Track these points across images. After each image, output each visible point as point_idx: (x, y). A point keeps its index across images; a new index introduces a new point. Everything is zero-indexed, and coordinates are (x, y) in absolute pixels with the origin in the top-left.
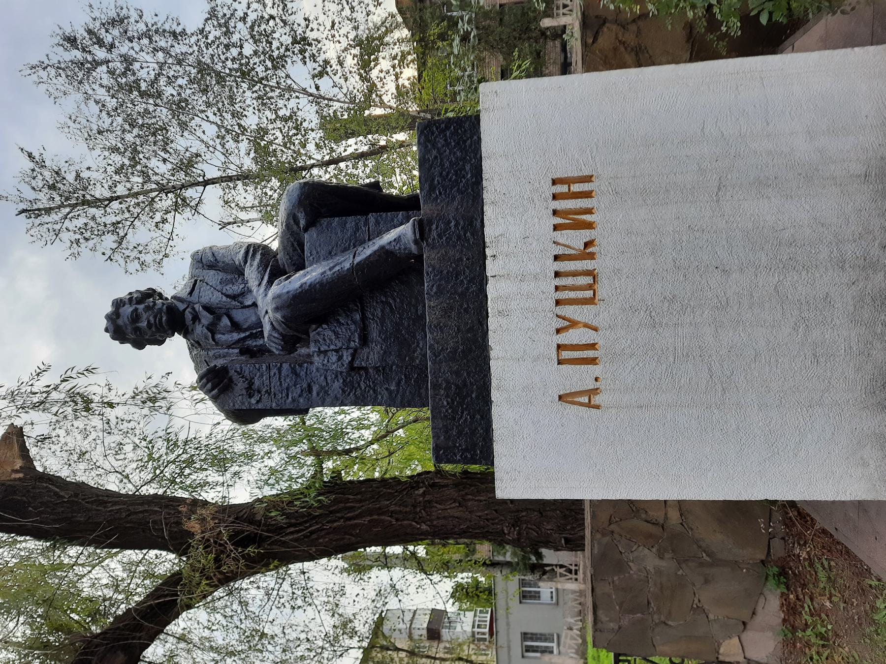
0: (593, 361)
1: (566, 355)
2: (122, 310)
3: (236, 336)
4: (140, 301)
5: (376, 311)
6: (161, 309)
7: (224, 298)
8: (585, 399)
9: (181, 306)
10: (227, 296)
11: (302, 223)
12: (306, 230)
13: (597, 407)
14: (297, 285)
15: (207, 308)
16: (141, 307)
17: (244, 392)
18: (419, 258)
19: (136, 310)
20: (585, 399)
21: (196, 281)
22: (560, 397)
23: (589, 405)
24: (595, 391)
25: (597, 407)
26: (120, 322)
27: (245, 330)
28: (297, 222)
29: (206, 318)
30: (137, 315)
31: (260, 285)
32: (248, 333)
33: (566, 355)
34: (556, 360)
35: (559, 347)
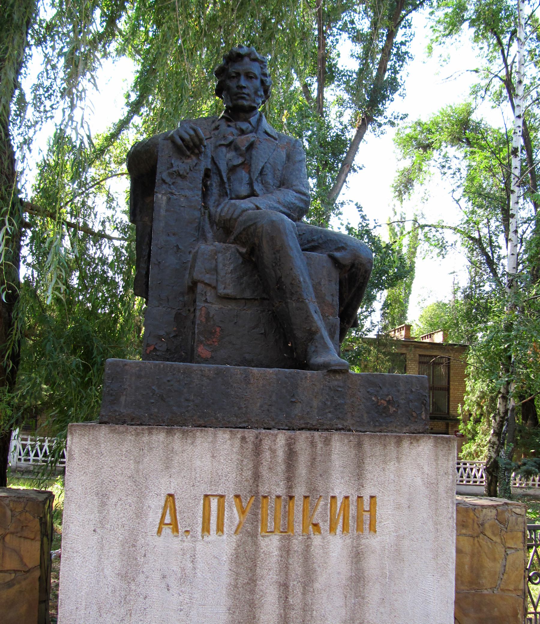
0: (206, 529)
1: (214, 503)
2: (257, 64)
3: (223, 168)
4: (263, 82)
5: (250, 313)
6: (254, 101)
7: (262, 165)
8: (168, 520)
9: (253, 120)
10: (263, 168)
11: (338, 254)
12: (332, 257)
13: (159, 532)
14: (291, 244)
15: (251, 146)
16: (258, 83)
17: (175, 169)
18: (305, 366)
19: (256, 78)
20: (168, 520)
21: (276, 139)
22: (171, 495)
23: (162, 522)
24: (176, 529)
25: (159, 532)
26: (247, 60)
27: (229, 179)
28: (338, 249)
29: (243, 141)
30: (251, 78)
31: (279, 202)
32: (225, 179)
33: (214, 503)
34: (209, 493)
35: (222, 496)
